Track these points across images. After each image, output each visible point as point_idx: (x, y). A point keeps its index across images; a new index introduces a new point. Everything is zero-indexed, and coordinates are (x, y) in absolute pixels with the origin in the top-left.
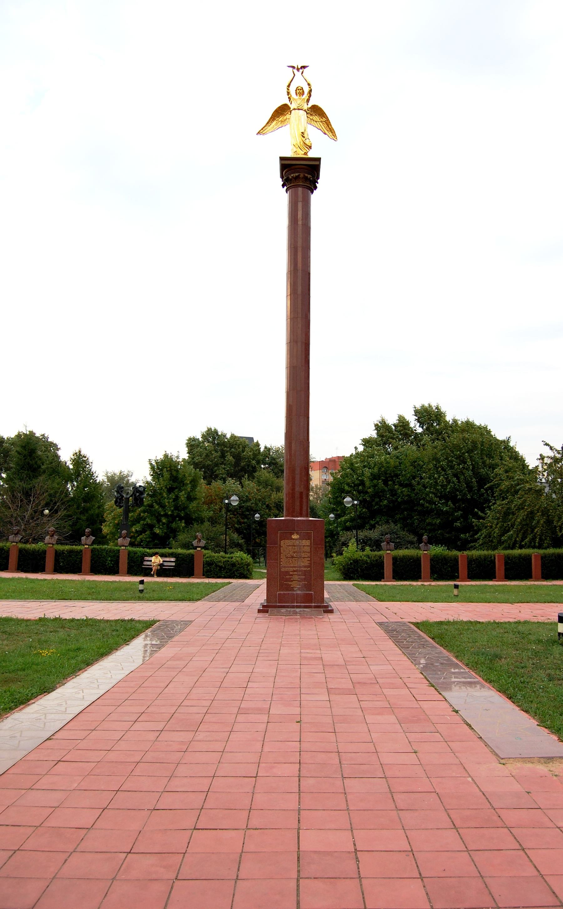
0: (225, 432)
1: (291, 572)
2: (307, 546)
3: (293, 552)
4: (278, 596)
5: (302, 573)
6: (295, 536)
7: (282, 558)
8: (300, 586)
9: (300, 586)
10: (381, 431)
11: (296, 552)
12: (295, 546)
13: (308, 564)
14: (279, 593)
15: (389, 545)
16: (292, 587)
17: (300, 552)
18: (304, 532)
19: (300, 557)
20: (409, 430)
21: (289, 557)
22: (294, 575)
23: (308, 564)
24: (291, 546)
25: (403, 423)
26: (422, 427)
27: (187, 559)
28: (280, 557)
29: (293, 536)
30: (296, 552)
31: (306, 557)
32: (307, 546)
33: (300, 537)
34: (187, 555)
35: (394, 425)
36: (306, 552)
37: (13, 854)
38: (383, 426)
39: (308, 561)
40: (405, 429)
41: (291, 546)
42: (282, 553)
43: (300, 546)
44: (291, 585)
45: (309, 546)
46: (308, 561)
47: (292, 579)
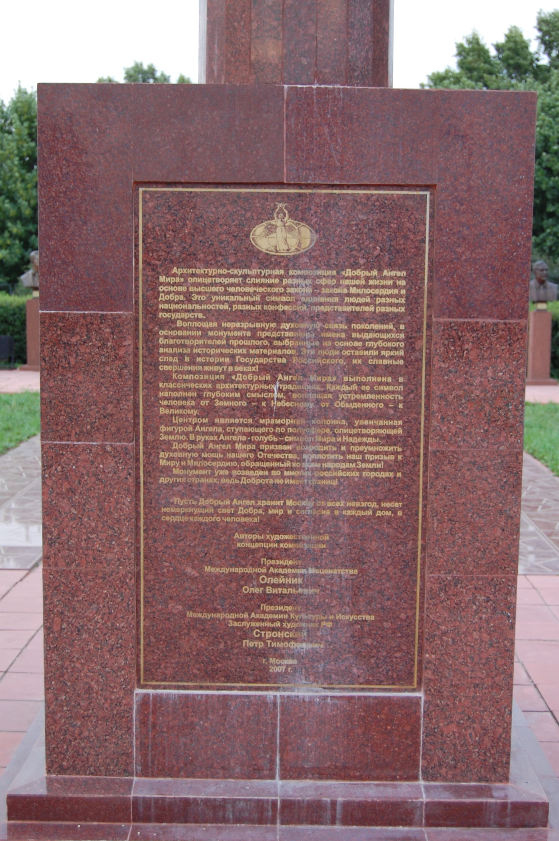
0: (167, 74)
1: (251, 529)
2: (384, 318)
3: (264, 369)
4: (143, 722)
5: (334, 545)
6: (280, 233)
7: (168, 420)
8: (319, 646)
9: (319, 646)
10: (470, 59)
11: (285, 369)
12: (277, 317)
13: (388, 467)
14: (145, 701)
15: (545, 288)
16: (251, 652)
17: (322, 370)
18: (355, 199)
19: (324, 413)
20: (525, 59)
21: (232, 412)
22: (268, 554)
23: (388, 467)
24: (243, 316)
25: (515, 42)
26: (549, 55)
27: (15, 321)
28: (149, 406)
29: (259, 230)
30: (285, 369)
31: (368, 415)
32: (384, 318)
33: (318, 245)
34: (14, 310)
35: (499, 48)
36: (374, 370)
37: (24, 577)
38: (472, 50)
39: (389, 440)
40: (517, 54)
41: (243, 316)
42: (167, 377)
43: (325, 318)
44: (246, 634)
45: (395, 318)
46: (389, 440)
47: (247, 590)
